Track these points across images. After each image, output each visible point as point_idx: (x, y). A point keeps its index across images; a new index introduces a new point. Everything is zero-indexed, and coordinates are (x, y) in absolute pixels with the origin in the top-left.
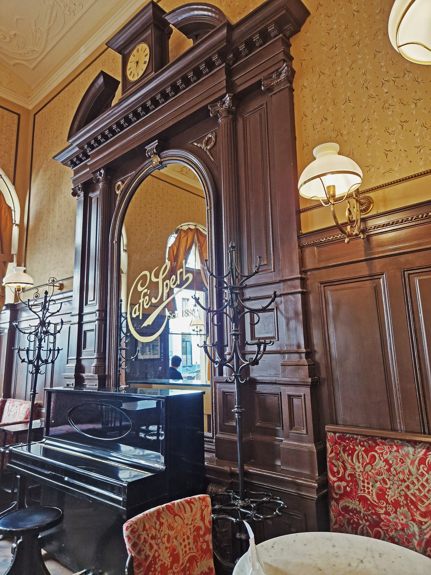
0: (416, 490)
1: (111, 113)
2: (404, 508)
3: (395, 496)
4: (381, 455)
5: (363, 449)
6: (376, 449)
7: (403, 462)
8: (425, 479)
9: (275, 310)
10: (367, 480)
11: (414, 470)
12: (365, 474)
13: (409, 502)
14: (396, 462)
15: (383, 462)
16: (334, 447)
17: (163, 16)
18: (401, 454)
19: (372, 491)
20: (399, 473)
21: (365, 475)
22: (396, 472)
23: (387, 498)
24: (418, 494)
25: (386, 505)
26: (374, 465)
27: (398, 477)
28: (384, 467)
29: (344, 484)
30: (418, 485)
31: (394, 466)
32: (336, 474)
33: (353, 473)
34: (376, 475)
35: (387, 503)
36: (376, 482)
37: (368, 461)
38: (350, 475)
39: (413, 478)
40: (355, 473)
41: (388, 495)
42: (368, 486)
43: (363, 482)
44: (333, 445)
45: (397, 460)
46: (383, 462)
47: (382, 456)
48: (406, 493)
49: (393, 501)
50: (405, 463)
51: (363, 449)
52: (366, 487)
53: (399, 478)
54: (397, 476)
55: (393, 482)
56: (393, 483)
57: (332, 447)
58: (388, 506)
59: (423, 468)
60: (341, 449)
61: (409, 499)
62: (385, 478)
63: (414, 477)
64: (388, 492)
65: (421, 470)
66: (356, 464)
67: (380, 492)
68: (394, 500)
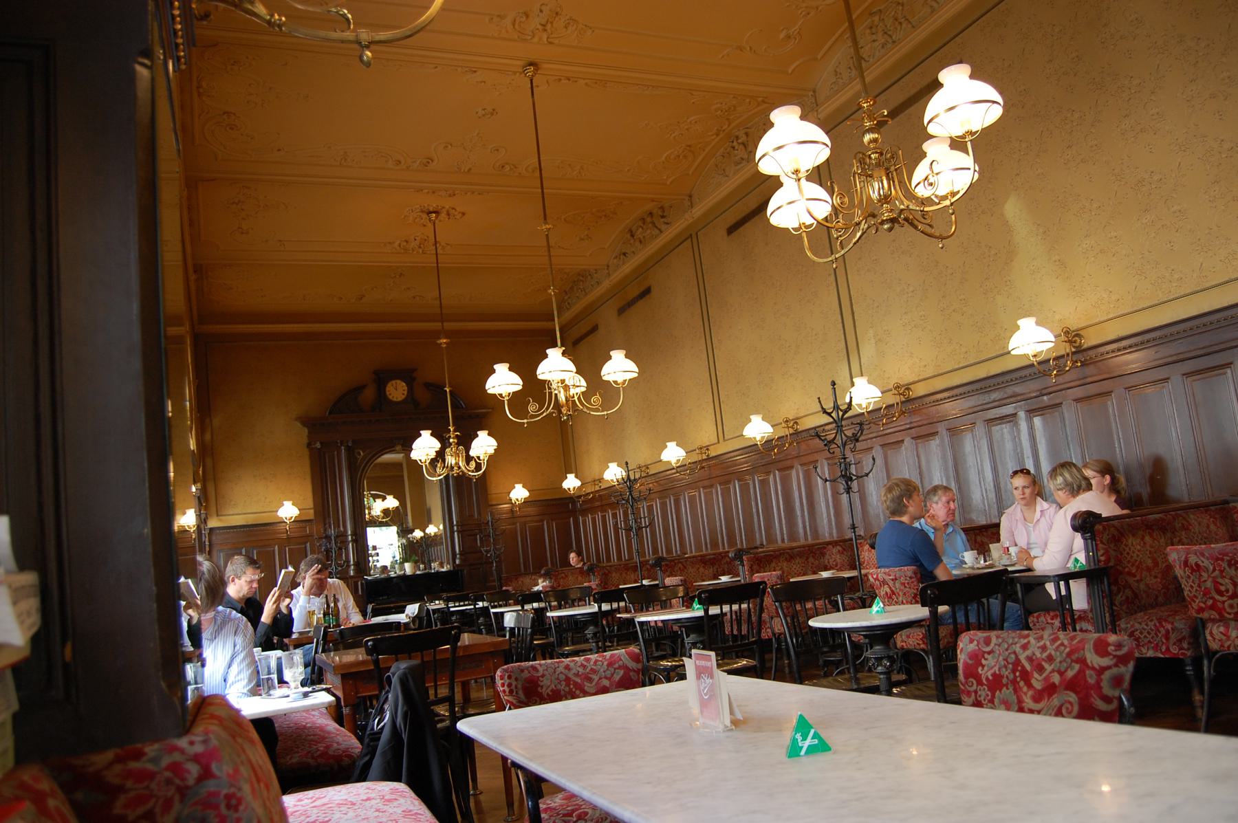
1: (737, 456)
2: (1007, 689)
9: (1046, 468)
13: (572, 686)
17: (320, 566)
19: (516, 687)
23: (980, 672)
25: (977, 686)
35: (980, 683)
41: (542, 687)
58: (980, 690)
60: (1225, 565)
64: (986, 659)
65: (1187, 573)
68: (551, 691)
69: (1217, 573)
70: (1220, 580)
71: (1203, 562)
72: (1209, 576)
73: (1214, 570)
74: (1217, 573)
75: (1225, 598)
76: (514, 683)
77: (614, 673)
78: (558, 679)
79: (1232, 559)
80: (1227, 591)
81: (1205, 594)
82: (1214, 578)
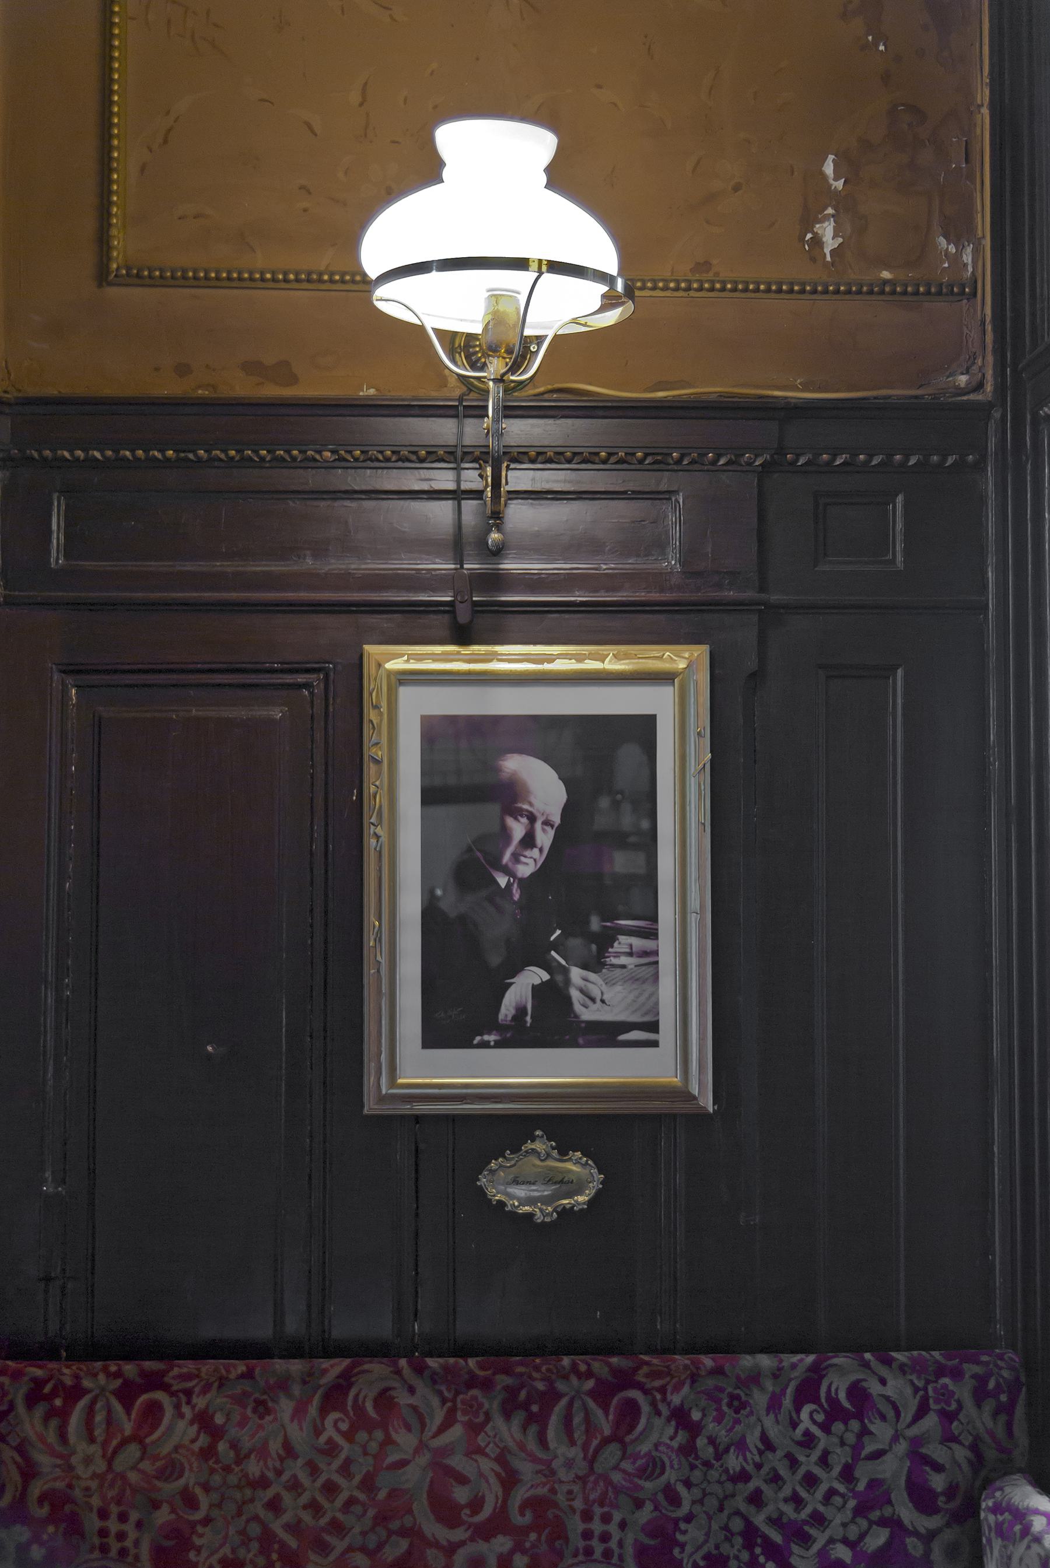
0: (786, 1500)
3: (706, 1541)
4: (658, 1397)
5: (590, 1384)
6: (166, 1379)
7: (744, 1405)
8: (816, 1454)
10: (119, 1503)
11: (298, 1434)
12: (596, 1483)
14: (716, 1410)
15: (669, 1420)
16: (935, 1390)
18: (262, 1384)
19: (621, 1544)
20: (727, 1450)
21: (112, 1486)
22: (716, 1448)
24: (793, 1515)
26: (153, 1443)
27: (722, 1466)
28: (193, 1441)
29: (502, 1543)
30: (792, 1483)
31: (711, 1427)
32: (467, 1511)
33: (545, 1490)
34: (640, 1478)
36: (156, 1505)
37: (128, 1428)
38: (531, 1504)
39: (297, 1469)
40: (553, 1491)
41: (682, 1546)
42: (606, 1528)
43: (103, 1514)
44: (928, 1382)
45: (718, 1401)
46: (669, 1420)
47: (664, 1400)
48: (748, 1523)
49: (702, 1563)
50: (748, 1409)
51: (590, 1384)
52: (597, 1533)
53: (727, 1471)
54: (237, 1469)
55: (704, 1490)
56: (705, 1494)
57: (925, 1389)
59: (811, 1414)
60: (963, 1391)
61: (759, 1541)
62: (191, 1485)
63: (780, 1453)
64: (684, 1532)
65: (330, 1432)
66: (559, 1452)
67: (652, 1542)
68: (705, 1558)
69: (931, 1421)
70: (458, 1462)
71: (883, 1382)
72: (421, 1447)
73: (922, 1411)
74: (931, 1421)
75: (459, 1534)
76: (132, 1535)
77: (386, 1542)
78: (726, 1528)
79: (522, 1386)
80: (476, 1505)
81: (382, 1519)
82: (916, 1442)
